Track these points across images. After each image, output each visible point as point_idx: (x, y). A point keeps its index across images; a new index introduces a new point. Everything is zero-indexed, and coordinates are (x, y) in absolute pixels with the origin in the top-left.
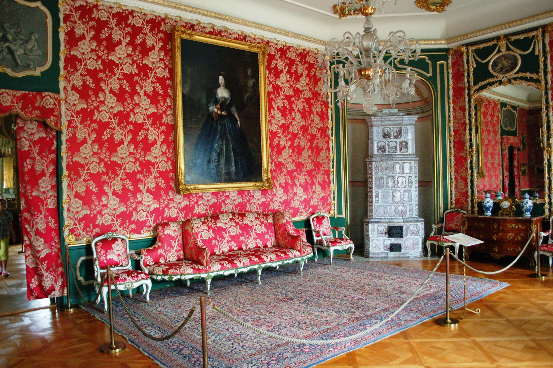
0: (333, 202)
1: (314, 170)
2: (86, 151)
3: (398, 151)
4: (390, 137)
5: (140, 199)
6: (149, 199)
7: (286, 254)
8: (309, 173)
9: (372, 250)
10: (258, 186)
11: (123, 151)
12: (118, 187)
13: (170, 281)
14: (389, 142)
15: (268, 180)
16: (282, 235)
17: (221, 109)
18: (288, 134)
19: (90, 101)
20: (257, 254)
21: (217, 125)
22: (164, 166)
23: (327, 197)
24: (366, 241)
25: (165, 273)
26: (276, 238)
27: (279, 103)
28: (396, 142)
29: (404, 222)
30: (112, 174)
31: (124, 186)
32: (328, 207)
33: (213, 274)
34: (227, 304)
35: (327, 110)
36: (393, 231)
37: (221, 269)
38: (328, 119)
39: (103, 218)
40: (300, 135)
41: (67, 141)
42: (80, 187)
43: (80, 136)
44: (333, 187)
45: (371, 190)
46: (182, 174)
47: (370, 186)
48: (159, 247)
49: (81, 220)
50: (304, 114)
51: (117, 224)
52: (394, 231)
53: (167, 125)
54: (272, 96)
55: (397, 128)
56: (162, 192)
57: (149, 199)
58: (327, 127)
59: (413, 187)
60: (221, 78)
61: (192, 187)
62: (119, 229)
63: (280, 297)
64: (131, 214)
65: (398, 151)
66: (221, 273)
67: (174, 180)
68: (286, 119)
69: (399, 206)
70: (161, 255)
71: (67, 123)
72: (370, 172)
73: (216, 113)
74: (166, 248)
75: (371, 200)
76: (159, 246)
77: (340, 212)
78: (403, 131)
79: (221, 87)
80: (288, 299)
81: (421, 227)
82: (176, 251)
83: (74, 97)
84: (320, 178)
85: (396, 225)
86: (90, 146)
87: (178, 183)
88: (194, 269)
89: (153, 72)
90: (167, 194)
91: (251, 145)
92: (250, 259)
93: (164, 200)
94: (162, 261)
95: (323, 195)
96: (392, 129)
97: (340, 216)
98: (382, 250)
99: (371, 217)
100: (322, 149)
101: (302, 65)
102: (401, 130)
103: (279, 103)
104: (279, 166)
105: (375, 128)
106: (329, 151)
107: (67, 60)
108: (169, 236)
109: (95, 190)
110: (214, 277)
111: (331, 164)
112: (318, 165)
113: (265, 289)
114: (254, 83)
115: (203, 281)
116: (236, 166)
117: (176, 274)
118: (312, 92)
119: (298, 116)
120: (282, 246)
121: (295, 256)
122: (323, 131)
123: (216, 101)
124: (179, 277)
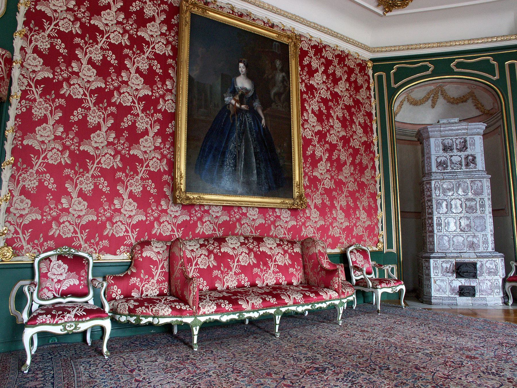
0: (381, 232)
1: (358, 191)
2: (45, 134)
3: (464, 167)
4: (452, 150)
5: (118, 206)
6: (131, 208)
7: (317, 294)
8: (352, 194)
9: (433, 294)
10: (287, 203)
11: (99, 139)
12: (88, 187)
13: (138, 325)
14: (452, 156)
15: (300, 197)
16: (312, 269)
17: (241, 102)
18: (325, 143)
19: (59, 70)
20: (275, 292)
21: (234, 120)
22: (156, 165)
23: (374, 227)
24: (425, 282)
25: (132, 312)
26: (305, 273)
27: (314, 105)
28: (460, 156)
29: (478, 257)
30: (80, 167)
31: (96, 186)
32: (375, 239)
33: (203, 319)
34: (211, 373)
35: (371, 122)
36: (463, 269)
37: (216, 312)
38: (373, 133)
39: (61, 228)
40: (340, 147)
41: (17, 116)
42: (30, 180)
43: (38, 112)
44: (381, 214)
45: (430, 216)
46: (181, 177)
47: (430, 211)
48: (133, 275)
49: (26, 228)
50: (345, 123)
51: (81, 237)
52: (464, 270)
53: (165, 113)
54: (305, 96)
55: (461, 138)
56: (152, 200)
57: (131, 208)
58: (372, 142)
59: (487, 212)
60: (241, 65)
61: (196, 196)
62: (84, 245)
63: (303, 364)
64: (103, 226)
65: (464, 167)
66: (217, 317)
67: (169, 184)
68: (322, 126)
69: (468, 236)
70: (134, 286)
71: (20, 92)
72: (429, 193)
73: (234, 106)
74: (142, 276)
75: (430, 229)
76: (132, 272)
77: (390, 246)
78: (468, 143)
79: (242, 75)
80: (317, 369)
81: (500, 263)
82: (158, 281)
83: (35, 63)
84: (365, 201)
85: (467, 260)
86: (51, 128)
87: (174, 188)
88: (174, 309)
89: (151, 47)
90: (158, 204)
91: (278, 151)
92: (264, 300)
93: (153, 211)
94: (135, 294)
95: (369, 223)
96: (454, 140)
97: (390, 250)
98: (448, 294)
99: (432, 251)
100: (367, 167)
101: (340, 67)
102: (465, 141)
103: (314, 105)
104: (314, 181)
105: (432, 140)
106: (375, 171)
107: (28, 14)
108: (149, 259)
109: (52, 187)
110: (205, 323)
111: (378, 186)
112: (362, 186)
113: (281, 347)
114: (283, 77)
115: (186, 328)
116: (258, 174)
117: (146, 316)
118: (358, 182)
119: (338, 125)
120: (313, 283)
121: (331, 298)
122: (368, 145)
123: (234, 92)
124: (150, 319)
